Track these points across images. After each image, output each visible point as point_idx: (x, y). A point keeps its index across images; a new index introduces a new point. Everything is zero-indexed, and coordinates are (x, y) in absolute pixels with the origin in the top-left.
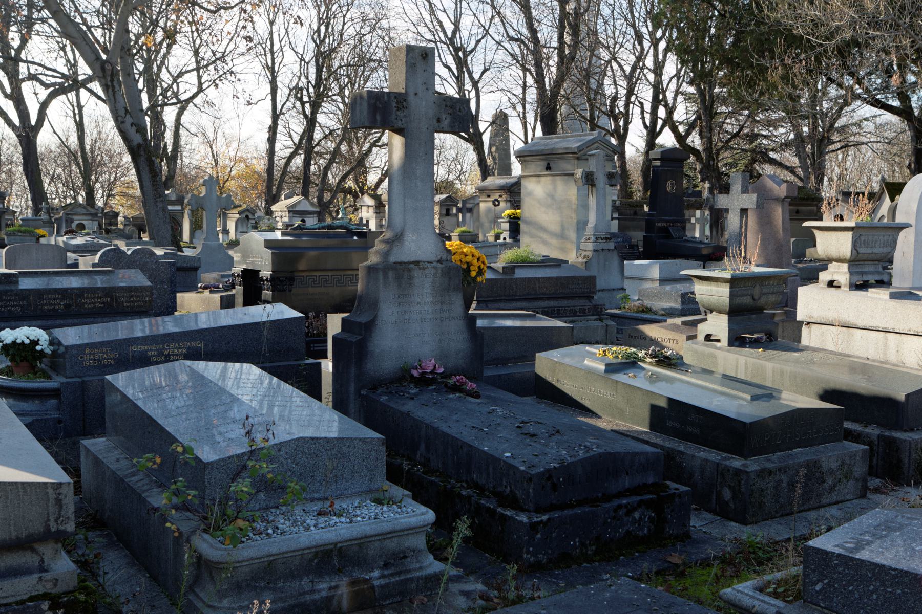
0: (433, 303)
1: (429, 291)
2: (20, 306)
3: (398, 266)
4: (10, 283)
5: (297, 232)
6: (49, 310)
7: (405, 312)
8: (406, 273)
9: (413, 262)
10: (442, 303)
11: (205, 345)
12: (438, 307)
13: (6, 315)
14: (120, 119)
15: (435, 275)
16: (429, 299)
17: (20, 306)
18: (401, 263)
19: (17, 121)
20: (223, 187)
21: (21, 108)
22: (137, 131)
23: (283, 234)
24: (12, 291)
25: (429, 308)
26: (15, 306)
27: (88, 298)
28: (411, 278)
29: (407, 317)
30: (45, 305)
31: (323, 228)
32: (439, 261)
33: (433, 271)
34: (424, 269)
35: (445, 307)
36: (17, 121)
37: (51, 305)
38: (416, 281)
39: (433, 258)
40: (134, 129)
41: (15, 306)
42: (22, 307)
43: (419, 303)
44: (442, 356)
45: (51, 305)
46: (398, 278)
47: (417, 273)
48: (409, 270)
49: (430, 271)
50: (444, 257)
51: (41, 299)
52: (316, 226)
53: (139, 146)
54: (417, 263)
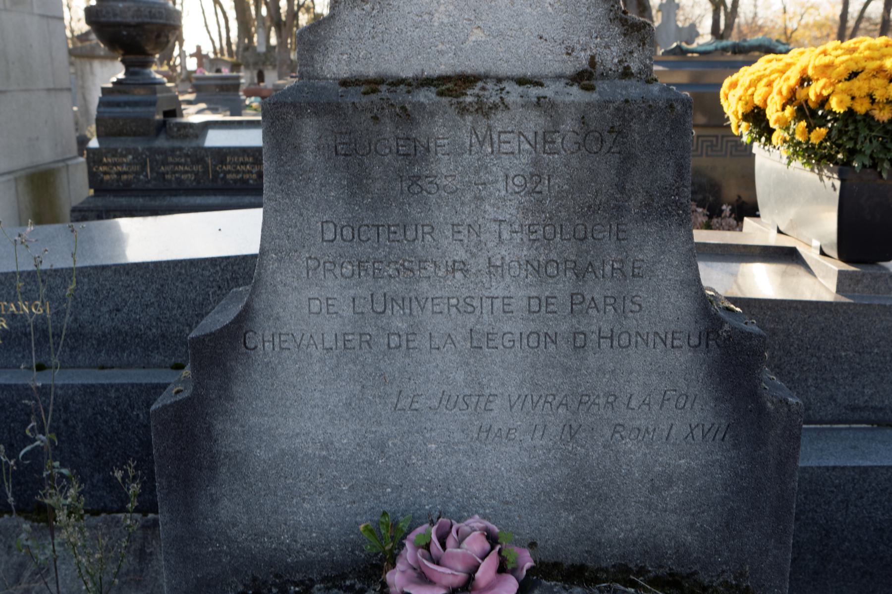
0: (539, 270)
1: (510, 211)
2: (192, 172)
3: (354, 96)
4: (186, 137)
5: (672, 58)
6: (235, 181)
7: (390, 300)
8: (388, 128)
9: (427, 82)
13: (174, 186)
15: (546, 138)
16: (511, 249)
17: (192, 172)
18: (373, 84)
20: (791, 37)
24: (181, 149)
25: (516, 289)
26: (186, 172)
28: (415, 154)
29: (399, 324)
30: (229, 172)
31: (724, 50)
32: (583, 78)
33: (534, 122)
34: (484, 110)
35: (595, 290)
37: (238, 172)
38: (443, 167)
39: (551, 61)
41: (186, 172)
42: (196, 174)
45: (238, 172)
46: (351, 156)
48: (405, 116)
49: (516, 126)
50: (610, 57)
51: (223, 162)
52: (711, 48)
54: (453, 85)
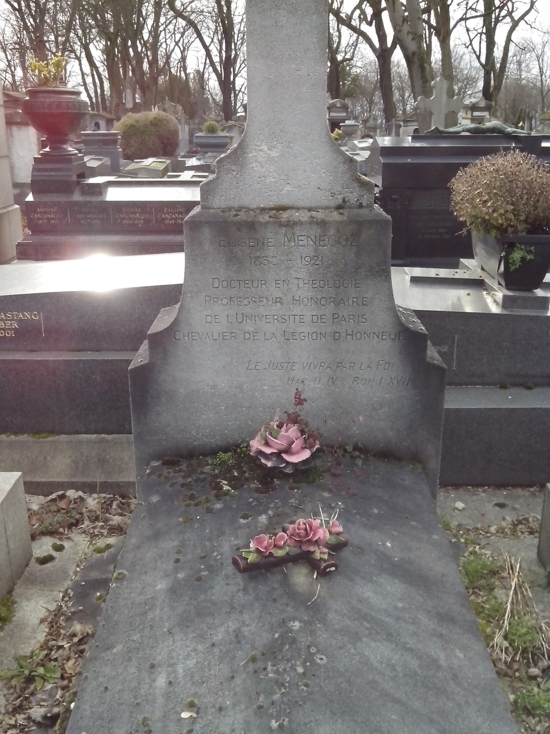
1: (303, 274)
6: (129, 225)
10: (338, 302)
11: (46, 318)
12: (330, 309)
14: (397, 27)
16: (305, 291)
19: (377, 45)
21: (381, 33)
22: (413, 39)
23: (414, 138)
27: (168, 213)
36: (377, 45)
37: (130, 219)
39: (323, 198)
40: (410, 37)
43: (278, 300)
44: (88, 503)
47: (272, 236)
53: (414, 54)
